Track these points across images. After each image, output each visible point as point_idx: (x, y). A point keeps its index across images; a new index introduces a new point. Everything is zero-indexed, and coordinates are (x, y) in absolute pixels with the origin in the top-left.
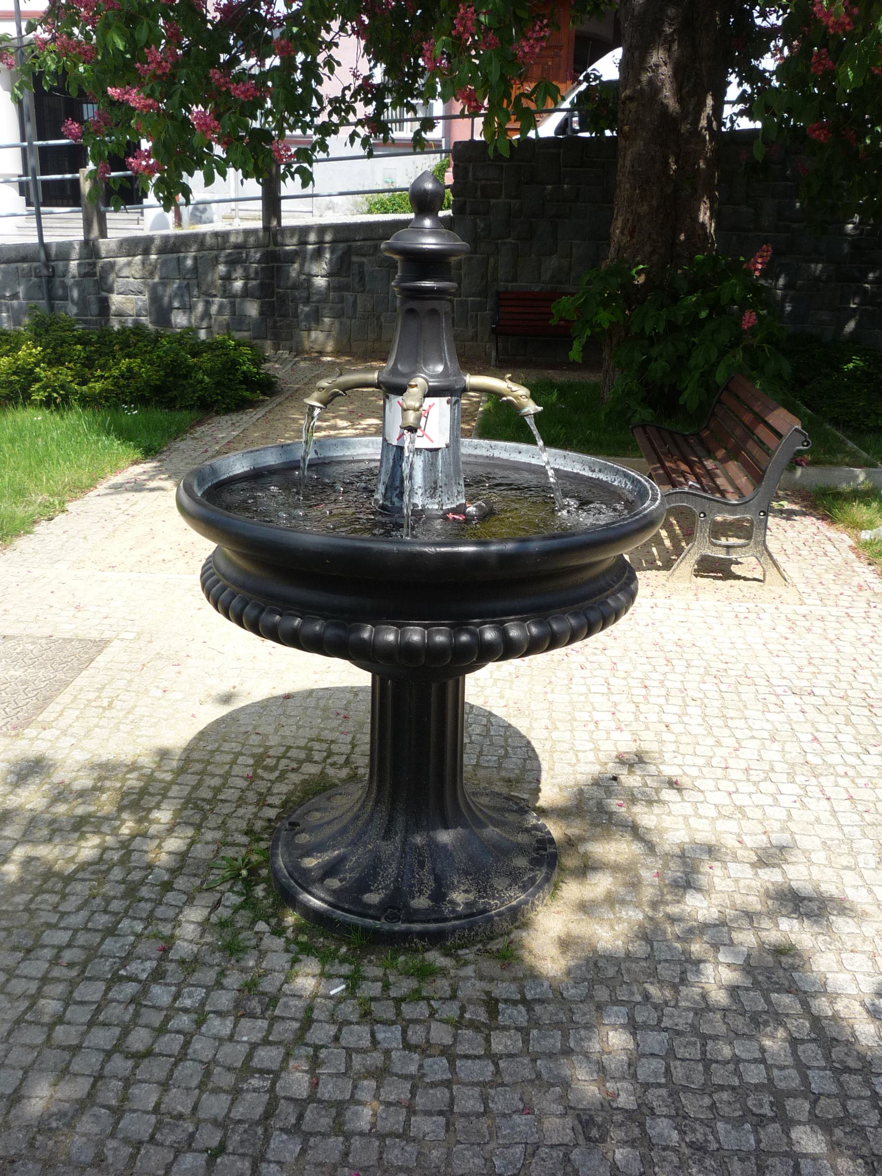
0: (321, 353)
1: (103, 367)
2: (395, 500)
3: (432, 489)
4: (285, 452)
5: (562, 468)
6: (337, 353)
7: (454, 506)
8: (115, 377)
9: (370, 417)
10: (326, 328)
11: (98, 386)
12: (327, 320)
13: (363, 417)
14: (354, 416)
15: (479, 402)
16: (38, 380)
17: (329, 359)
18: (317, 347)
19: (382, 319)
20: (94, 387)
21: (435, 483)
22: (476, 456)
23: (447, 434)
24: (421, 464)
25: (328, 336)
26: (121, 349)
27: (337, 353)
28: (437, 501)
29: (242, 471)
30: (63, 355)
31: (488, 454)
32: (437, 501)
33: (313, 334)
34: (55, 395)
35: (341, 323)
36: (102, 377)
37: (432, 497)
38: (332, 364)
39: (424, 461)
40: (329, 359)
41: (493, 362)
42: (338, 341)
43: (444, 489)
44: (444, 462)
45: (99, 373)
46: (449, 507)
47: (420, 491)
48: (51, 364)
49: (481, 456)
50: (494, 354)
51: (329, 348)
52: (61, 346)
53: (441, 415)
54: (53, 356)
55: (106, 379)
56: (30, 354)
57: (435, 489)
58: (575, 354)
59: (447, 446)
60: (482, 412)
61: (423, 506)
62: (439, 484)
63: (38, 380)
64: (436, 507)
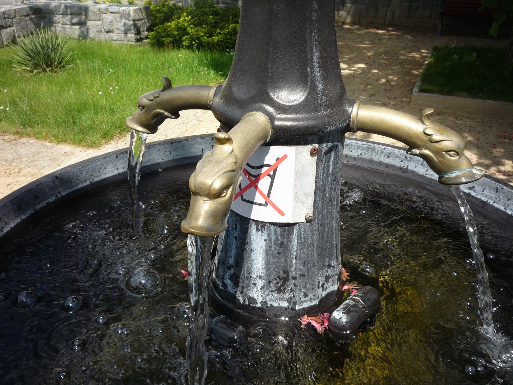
0: (344, 23)
1: (221, 28)
2: (228, 282)
3: (280, 280)
4: (176, 149)
5: (491, 202)
6: (352, 23)
7: (315, 302)
8: (225, 34)
9: (360, 63)
10: (348, 9)
11: (216, 38)
12: (348, 5)
13: (356, 62)
14: (352, 62)
15: (426, 57)
16: (187, 34)
17: (347, 26)
18: (342, 20)
19: (379, 5)
20: (214, 39)
21: (286, 272)
22: (387, 166)
23: (310, 202)
24: (263, 244)
25: (348, 14)
26: (233, 18)
27: (352, 23)
28: (287, 296)
29: (116, 172)
30: (203, 21)
31: (402, 165)
32: (287, 296)
33: (341, 13)
34: (194, 43)
35: (356, 8)
36: (220, 33)
37: (279, 290)
38: (348, 29)
39: (268, 241)
40: (347, 26)
41: (439, 32)
42: (353, 17)
43: (300, 281)
44: (301, 245)
45: (218, 31)
46: (306, 305)
47: (260, 283)
48: (196, 26)
49: (394, 167)
50: (440, 27)
51: (348, 20)
52: (203, 16)
53: (298, 175)
54: (199, 21)
55: (222, 34)
56: (185, 20)
57: (285, 280)
58: (493, 31)
59: (309, 221)
60: (427, 65)
61: (264, 303)
62: (293, 273)
63: (187, 34)
64: (285, 304)
